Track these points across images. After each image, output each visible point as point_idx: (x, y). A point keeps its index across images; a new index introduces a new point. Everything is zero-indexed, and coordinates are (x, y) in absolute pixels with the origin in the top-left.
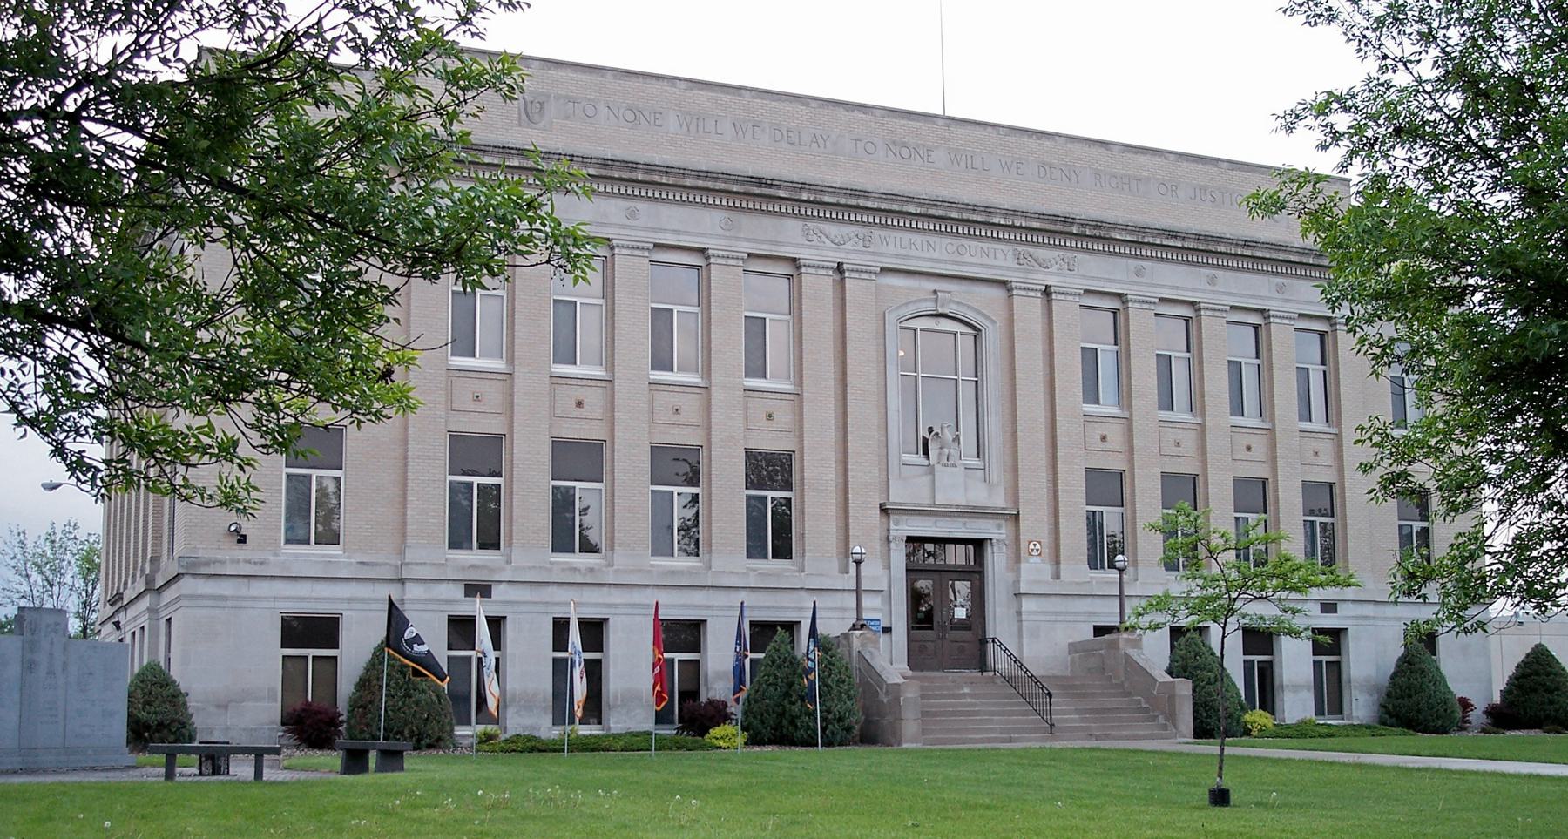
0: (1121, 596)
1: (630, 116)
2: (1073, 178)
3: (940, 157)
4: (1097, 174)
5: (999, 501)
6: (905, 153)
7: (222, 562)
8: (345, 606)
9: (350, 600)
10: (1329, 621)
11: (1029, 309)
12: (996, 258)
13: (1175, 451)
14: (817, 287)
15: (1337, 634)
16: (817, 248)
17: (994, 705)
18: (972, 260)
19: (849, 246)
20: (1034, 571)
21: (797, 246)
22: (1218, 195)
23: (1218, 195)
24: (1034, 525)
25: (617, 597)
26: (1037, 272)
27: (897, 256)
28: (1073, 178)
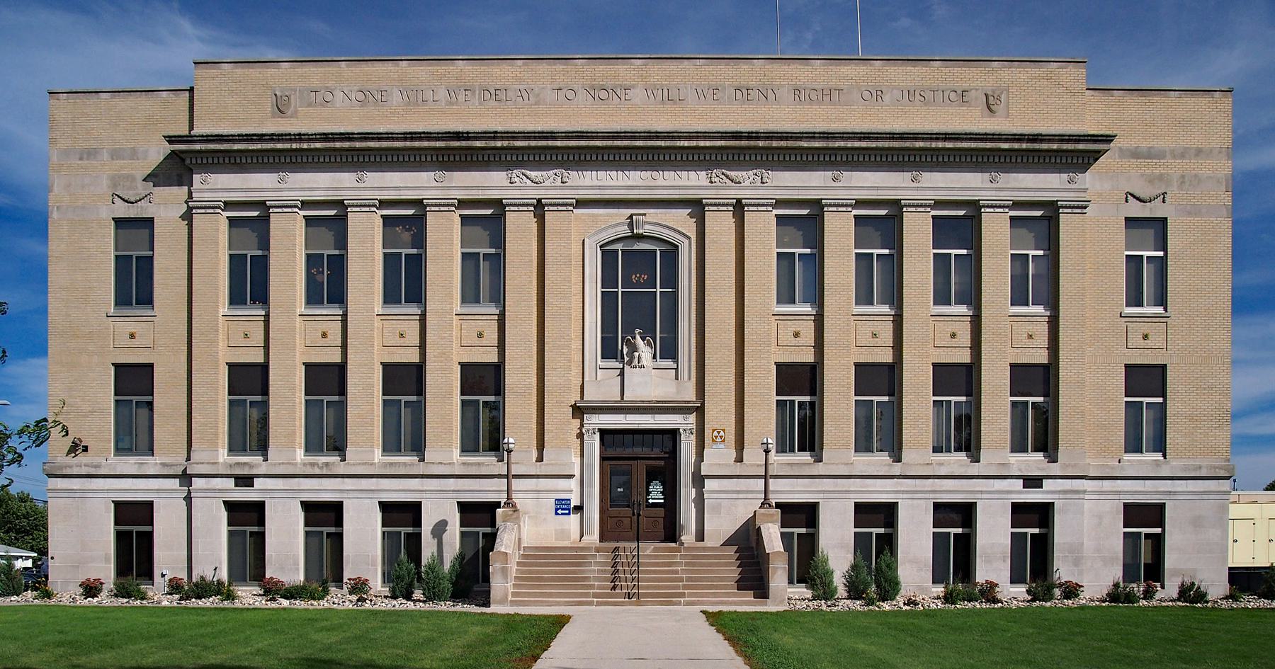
0: (507, 477)
1: (360, 96)
2: (771, 95)
3: (637, 95)
4: (797, 90)
5: (690, 394)
6: (603, 94)
7: (71, 467)
8: (1056, 496)
9: (158, 491)
10: (1033, 496)
11: (720, 225)
12: (693, 182)
13: (872, 342)
14: (720, 225)
15: (259, 508)
16: (519, 188)
17: (583, 572)
18: (665, 183)
19: (547, 183)
20: (718, 456)
21: (502, 188)
22: (929, 95)
23: (929, 95)
24: (720, 414)
25: (349, 484)
26: (729, 188)
27: (592, 187)
28: (771, 95)
